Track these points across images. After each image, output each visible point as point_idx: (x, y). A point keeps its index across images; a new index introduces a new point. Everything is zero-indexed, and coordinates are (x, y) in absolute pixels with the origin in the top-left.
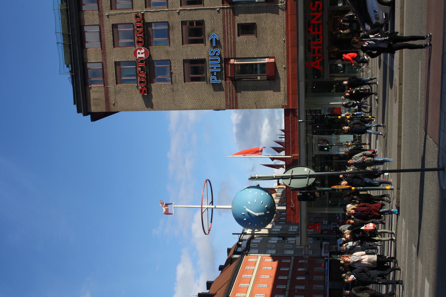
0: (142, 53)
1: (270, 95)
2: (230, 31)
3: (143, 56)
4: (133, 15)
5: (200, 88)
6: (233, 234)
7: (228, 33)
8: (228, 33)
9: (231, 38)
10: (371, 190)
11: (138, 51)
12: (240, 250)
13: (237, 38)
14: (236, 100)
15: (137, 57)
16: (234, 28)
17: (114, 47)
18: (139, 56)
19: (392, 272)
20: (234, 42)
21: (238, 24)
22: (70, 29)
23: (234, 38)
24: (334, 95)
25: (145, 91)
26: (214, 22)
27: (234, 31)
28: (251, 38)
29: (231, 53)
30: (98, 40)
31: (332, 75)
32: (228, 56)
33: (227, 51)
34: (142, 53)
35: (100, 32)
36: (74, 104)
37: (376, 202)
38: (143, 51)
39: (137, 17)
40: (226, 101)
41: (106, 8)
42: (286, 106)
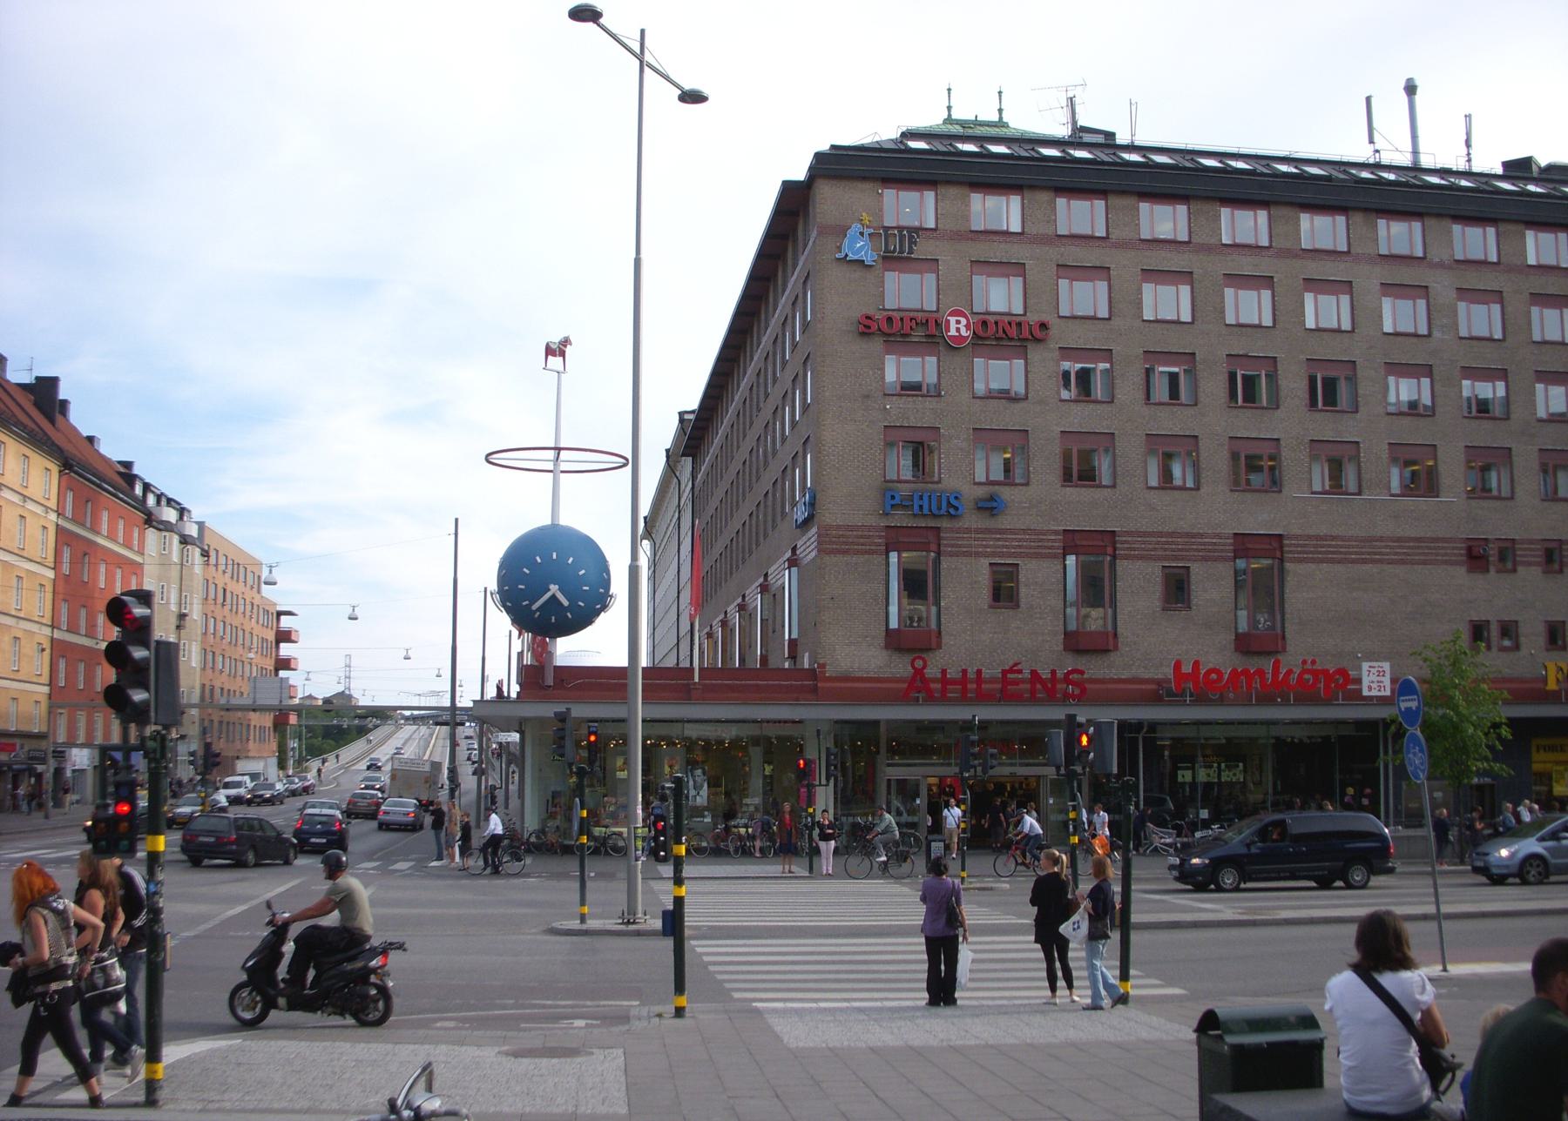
0: (958, 330)
1: (850, 636)
2: (1003, 546)
3: (953, 332)
4: (1044, 318)
5: (871, 464)
6: (457, 520)
7: (999, 539)
8: (999, 539)
9: (986, 546)
10: (1048, 965)
11: (964, 321)
12: (151, 500)
13: (985, 562)
14: (839, 552)
15: (949, 315)
16: (1010, 555)
17: (1058, 265)
18: (953, 320)
19: (780, 1026)
20: (977, 554)
21: (1018, 564)
22: (883, 155)
23: (986, 555)
24: (62, 665)
25: (870, 328)
26: (1025, 507)
27: (1002, 555)
28: (985, 593)
29: (952, 546)
30: (989, 227)
31: (893, 784)
32: (946, 539)
33: (958, 535)
34: (958, 330)
35: (1092, 237)
36: (833, 147)
37: (943, 967)
38: (964, 333)
39: (1043, 326)
40: (838, 527)
41: (1062, 255)
42: (824, 673)
